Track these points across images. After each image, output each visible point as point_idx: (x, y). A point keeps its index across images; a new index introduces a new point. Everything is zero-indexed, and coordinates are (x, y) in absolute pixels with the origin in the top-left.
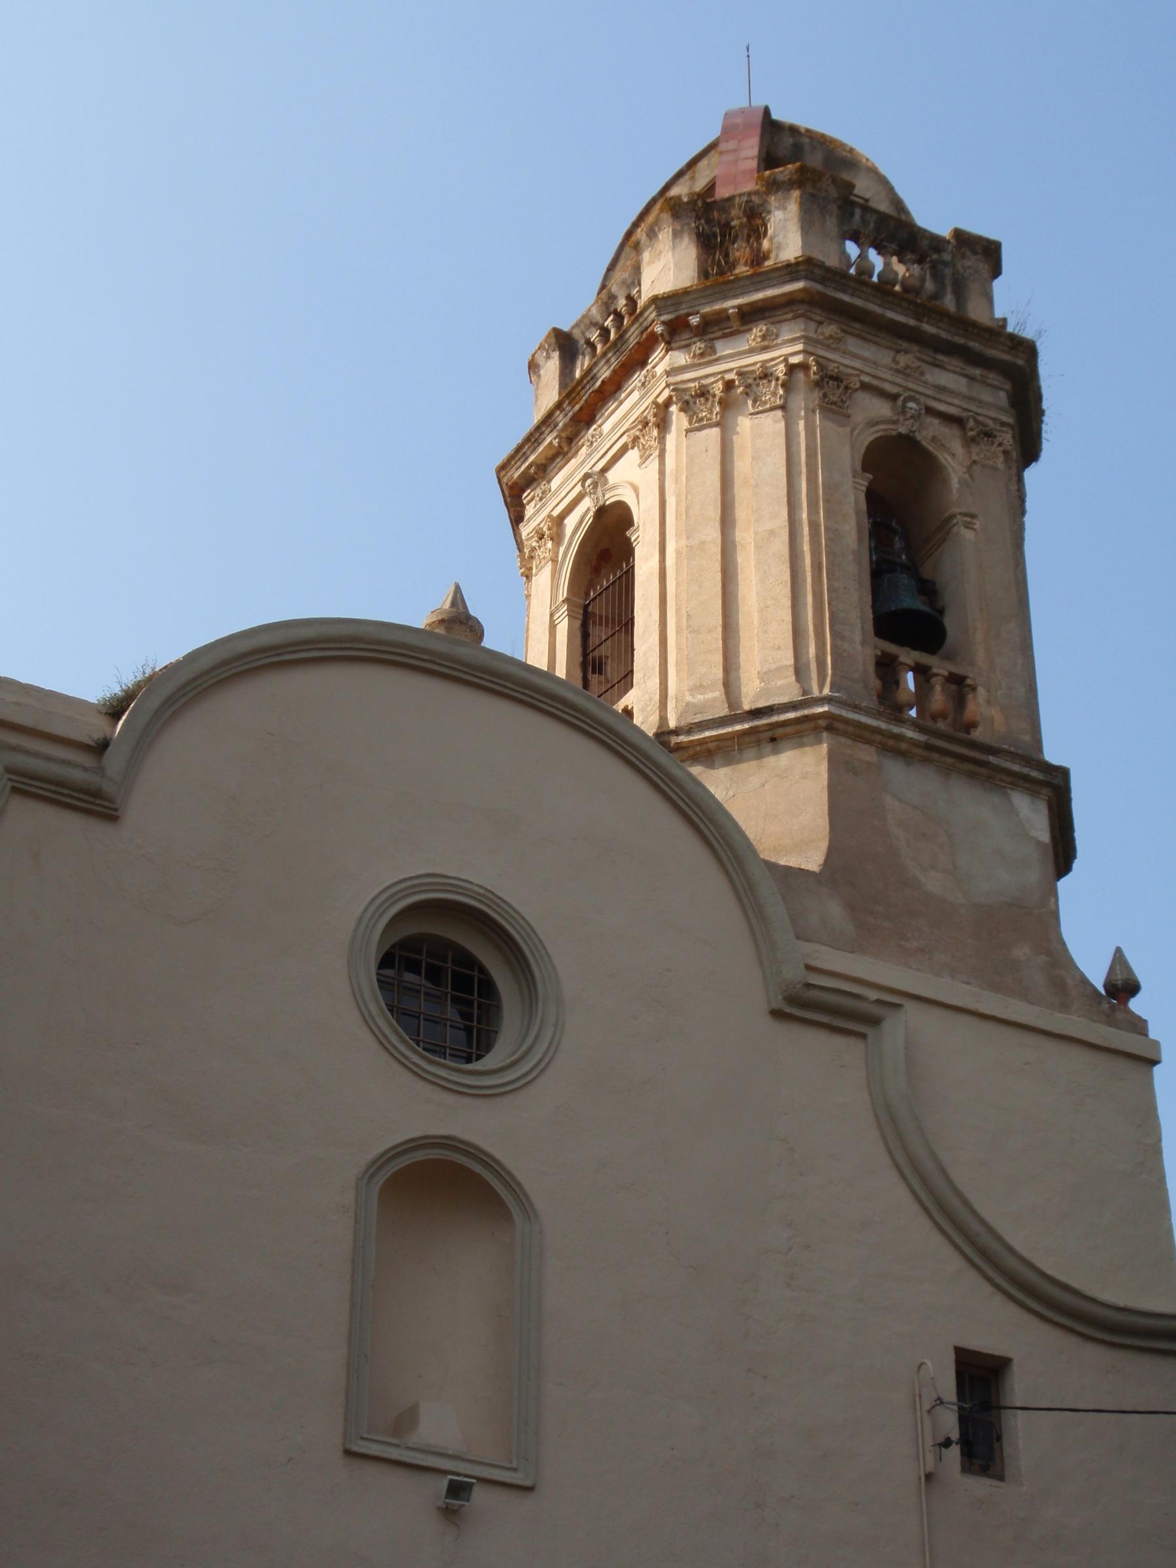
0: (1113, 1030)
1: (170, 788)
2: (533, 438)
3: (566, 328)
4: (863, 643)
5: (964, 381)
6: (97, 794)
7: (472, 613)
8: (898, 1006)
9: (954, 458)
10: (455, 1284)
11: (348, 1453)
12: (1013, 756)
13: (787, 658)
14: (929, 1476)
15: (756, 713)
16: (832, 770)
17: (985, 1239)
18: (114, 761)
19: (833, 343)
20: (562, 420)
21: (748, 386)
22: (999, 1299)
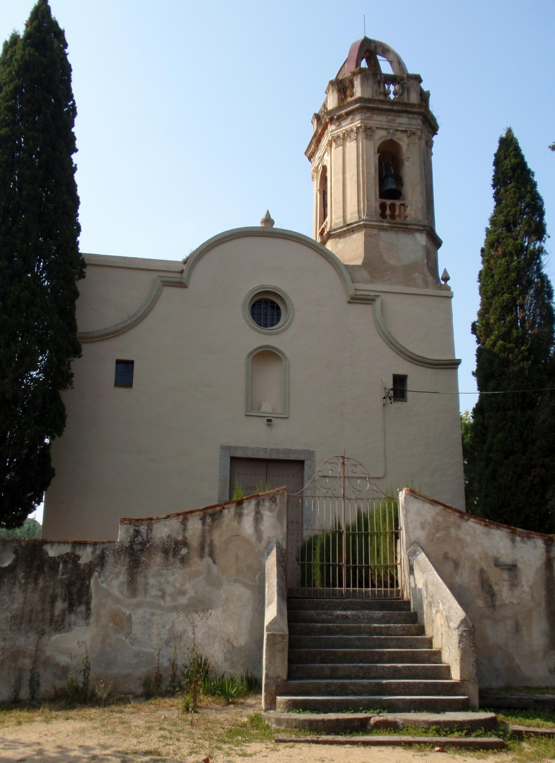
0: (440, 291)
1: (198, 279)
2: (310, 146)
3: (317, 112)
4: (376, 201)
5: (407, 119)
6: (181, 283)
7: (272, 218)
8: (379, 296)
9: (404, 142)
10: (271, 376)
11: (246, 415)
12: (415, 225)
13: (356, 209)
14: (384, 404)
15: (348, 225)
16: (365, 238)
17: (401, 348)
18: (185, 275)
19: (370, 118)
20: (314, 142)
21: (348, 134)
22: (405, 361)
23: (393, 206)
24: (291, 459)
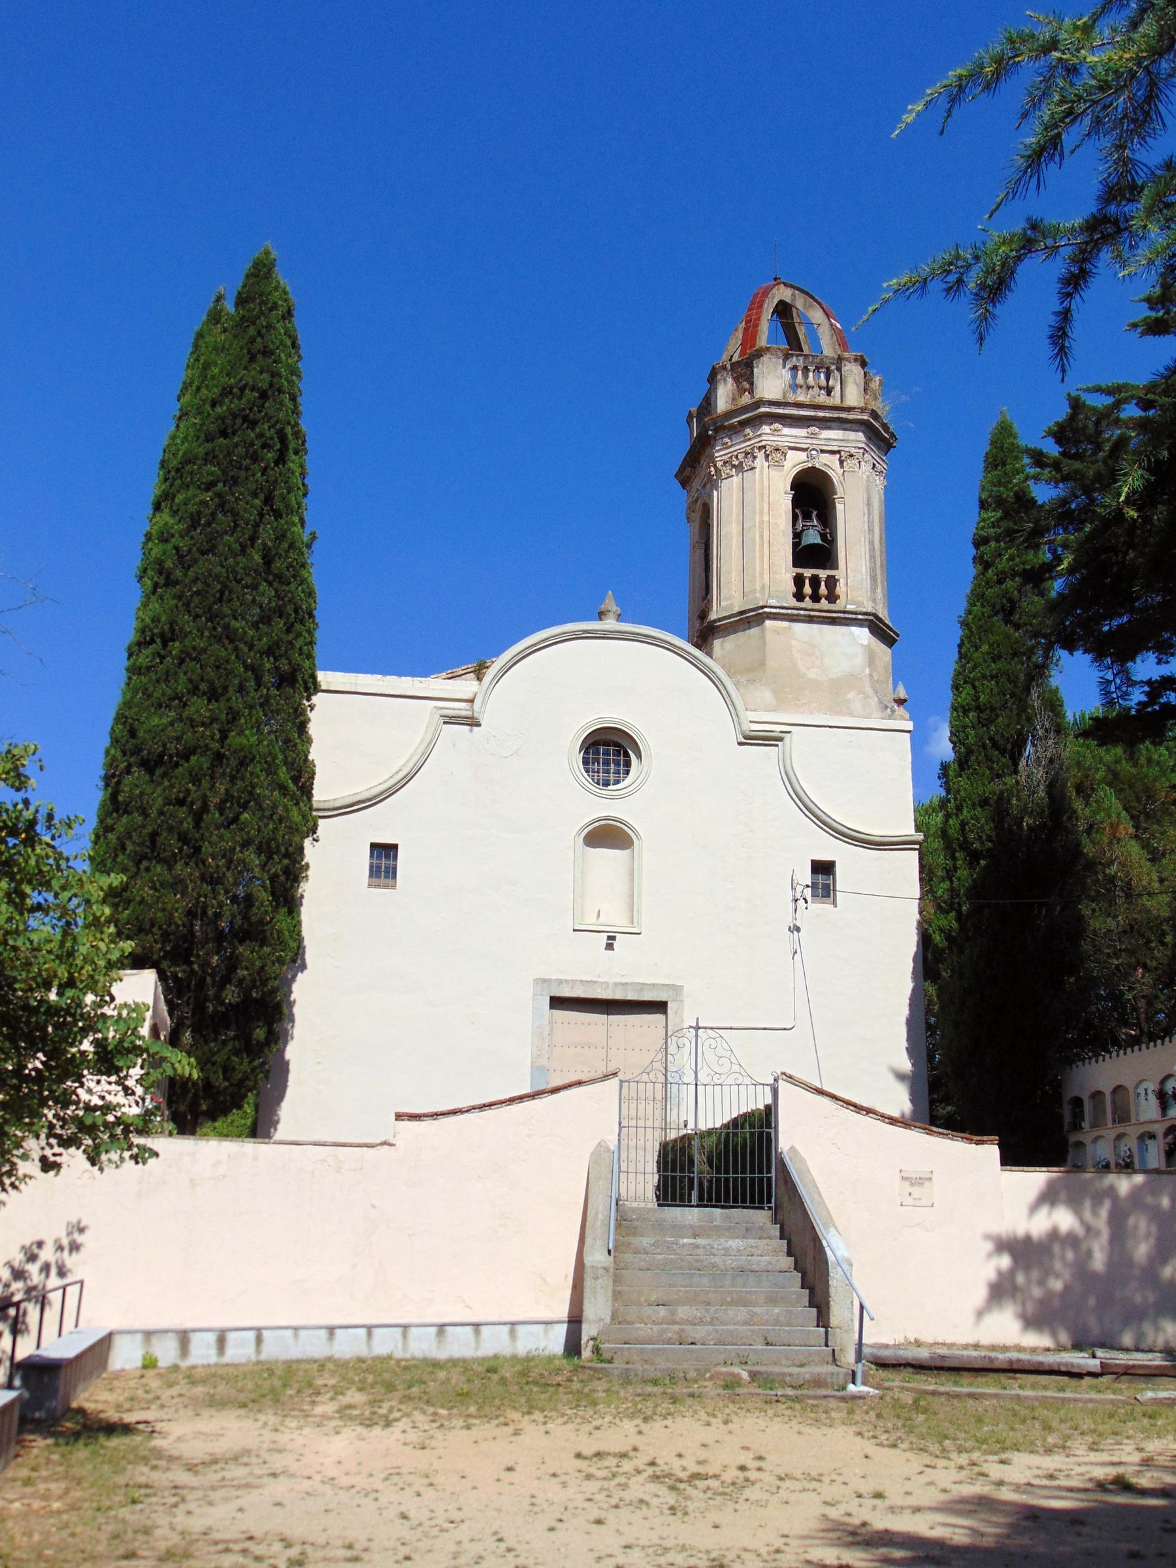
6: (472, 718)
23: (815, 581)
24: (646, 999)
